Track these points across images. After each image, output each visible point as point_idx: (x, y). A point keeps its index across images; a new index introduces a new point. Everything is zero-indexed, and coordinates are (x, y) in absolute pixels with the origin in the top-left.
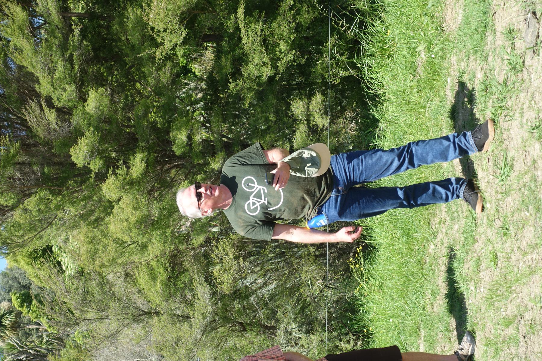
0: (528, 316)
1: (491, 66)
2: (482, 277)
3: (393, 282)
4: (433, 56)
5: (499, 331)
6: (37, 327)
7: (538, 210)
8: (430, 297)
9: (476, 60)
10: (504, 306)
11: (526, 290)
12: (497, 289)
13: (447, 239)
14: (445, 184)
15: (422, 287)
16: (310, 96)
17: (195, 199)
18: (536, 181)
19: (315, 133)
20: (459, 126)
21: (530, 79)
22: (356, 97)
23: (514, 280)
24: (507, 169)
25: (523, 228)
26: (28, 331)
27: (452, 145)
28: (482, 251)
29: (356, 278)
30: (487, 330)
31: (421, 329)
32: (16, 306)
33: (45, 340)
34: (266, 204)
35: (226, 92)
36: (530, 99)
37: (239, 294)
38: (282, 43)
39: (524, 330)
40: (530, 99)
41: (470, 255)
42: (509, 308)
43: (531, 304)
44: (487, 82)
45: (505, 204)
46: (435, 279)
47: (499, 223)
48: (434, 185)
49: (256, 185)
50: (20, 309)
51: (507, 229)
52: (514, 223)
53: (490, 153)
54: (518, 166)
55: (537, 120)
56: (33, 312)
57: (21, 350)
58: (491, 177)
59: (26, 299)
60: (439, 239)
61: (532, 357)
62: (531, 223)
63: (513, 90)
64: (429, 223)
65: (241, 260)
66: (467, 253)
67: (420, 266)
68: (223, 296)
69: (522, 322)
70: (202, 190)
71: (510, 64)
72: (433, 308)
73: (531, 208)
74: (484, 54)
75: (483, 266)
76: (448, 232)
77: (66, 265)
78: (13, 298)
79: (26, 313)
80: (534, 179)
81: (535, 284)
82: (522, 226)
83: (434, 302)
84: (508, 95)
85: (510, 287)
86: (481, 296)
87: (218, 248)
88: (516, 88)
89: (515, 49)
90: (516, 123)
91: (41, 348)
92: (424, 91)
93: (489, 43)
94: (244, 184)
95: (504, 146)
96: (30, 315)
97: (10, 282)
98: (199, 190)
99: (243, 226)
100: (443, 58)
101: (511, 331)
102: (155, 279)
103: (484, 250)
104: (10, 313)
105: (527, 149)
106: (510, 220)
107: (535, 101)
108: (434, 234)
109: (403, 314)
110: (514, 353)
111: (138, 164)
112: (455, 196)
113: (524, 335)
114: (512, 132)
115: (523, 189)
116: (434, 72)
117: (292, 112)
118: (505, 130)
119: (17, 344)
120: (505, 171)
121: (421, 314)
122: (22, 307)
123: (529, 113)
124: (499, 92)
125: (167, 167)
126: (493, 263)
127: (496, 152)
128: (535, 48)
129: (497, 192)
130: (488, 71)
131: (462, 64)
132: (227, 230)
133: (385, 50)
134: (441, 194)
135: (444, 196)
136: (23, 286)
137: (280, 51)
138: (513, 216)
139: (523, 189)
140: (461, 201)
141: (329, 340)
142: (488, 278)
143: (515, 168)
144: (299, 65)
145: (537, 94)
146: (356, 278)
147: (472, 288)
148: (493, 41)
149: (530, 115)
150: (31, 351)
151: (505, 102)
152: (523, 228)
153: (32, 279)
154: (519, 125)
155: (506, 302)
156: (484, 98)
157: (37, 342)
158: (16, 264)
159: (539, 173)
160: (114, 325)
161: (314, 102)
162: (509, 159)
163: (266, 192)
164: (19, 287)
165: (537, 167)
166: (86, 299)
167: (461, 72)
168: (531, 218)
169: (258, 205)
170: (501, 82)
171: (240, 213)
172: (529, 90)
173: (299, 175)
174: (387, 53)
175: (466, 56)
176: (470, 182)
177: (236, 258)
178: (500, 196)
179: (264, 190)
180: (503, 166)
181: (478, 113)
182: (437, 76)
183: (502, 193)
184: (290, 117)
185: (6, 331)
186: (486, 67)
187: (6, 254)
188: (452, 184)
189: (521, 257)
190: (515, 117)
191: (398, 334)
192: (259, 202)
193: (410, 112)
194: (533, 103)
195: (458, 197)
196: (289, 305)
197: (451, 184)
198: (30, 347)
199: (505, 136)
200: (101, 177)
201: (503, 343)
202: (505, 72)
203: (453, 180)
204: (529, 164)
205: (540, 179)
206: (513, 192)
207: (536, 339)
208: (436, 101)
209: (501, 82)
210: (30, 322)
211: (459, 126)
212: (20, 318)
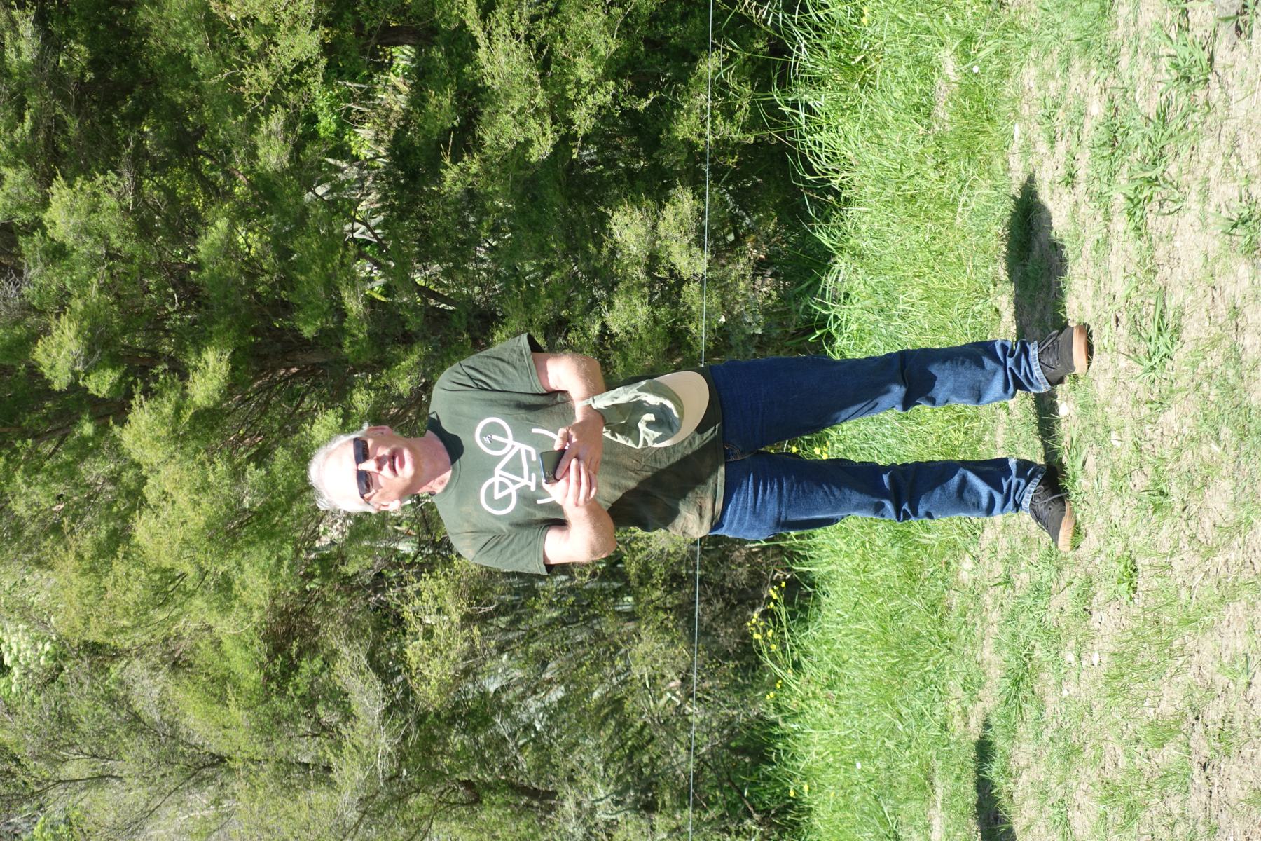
0: (1213, 713)
1: (1128, 81)
3: (865, 668)
4: (976, 69)
5: (1137, 761)
7: (1244, 434)
8: (960, 693)
9: (1087, 69)
10: (1151, 693)
11: (1208, 645)
12: (1136, 652)
13: (1005, 540)
14: (988, 472)
15: (940, 670)
16: (661, 197)
18: (1239, 360)
21: (1228, 100)
22: (778, 194)
24: (1167, 336)
28: (1098, 561)
31: (936, 779)
34: (533, 489)
36: (1228, 151)
39: (1203, 747)
40: (1228, 151)
41: (1066, 576)
43: (1222, 680)
44: (1117, 121)
46: (974, 645)
47: (1140, 481)
49: (510, 441)
51: (1162, 493)
54: (1194, 329)
55: (1244, 204)
60: (985, 543)
62: (1224, 472)
66: (1059, 569)
67: (935, 617)
69: (1199, 728)
70: (370, 466)
71: (1176, 66)
72: (966, 724)
73: (1226, 431)
74: (1107, 51)
75: (1101, 595)
77: (15, 651)
80: (1235, 356)
81: (1234, 627)
82: (1201, 480)
83: (971, 707)
85: (1168, 643)
88: (1191, 126)
89: (1188, 30)
90: (1191, 217)
92: (952, 164)
93: (1121, 23)
95: (1158, 280)
100: (1003, 74)
101: (1171, 753)
103: (1103, 556)
105: (1218, 281)
106: (1171, 470)
107: (1239, 156)
109: (890, 744)
111: (209, 376)
112: (1011, 504)
113: (1203, 760)
114: (1178, 244)
115: (1205, 385)
117: (611, 235)
118: (1161, 239)
123: (1223, 188)
124: (1146, 142)
125: (292, 361)
126: (1125, 586)
127: (1136, 300)
128: (1240, 18)
131: (1052, 84)
132: (437, 551)
133: (852, 69)
134: (977, 494)
135: (985, 502)
137: (579, 84)
138: (1178, 460)
139: (1205, 385)
143: (1184, 335)
144: (629, 114)
145: (1244, 137)
147: (1071, 657)
148: (1131, 16)
149: (1226, 193)
154: (1197, 223)
155: (1158, 682)
156: (1108, 163)
159: (1248, 340)
160: (137, 795)
162: (1170, 314)
165: (1241, 325)
167: (1049, 102)
169: (512, 490)
170: (1153, 116)
172: (1224, 129)
174: (855, 70)
179: (528, 453)
180: (1153, 332)
182: (986, 123)
183: (1152, 402)
189: (1197, 560)
190: (1187, 204)
191: (876, 799)
192: (515, 482)
193: (900, 280)
194: (1234, 160)
195: (1017, 507)
196: (592, 751)
197: (1007, 472)
199: (1160, 255)
200: (114, 410)
201: (1149, 788)
202: (1162, 87)
203: (1012, 463)
205: (1250, 356)
206: (1179, 396)
207: (1235, 768)
209: (1153, 116)
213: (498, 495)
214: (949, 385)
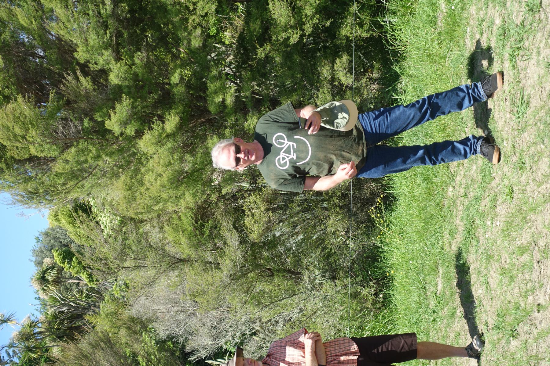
0: (542, 243)
1: (510, 11)
4: (453, 7)
5: (513, 260)
6: (78, 281)
9: (494, 7)
10: (519, 236)
11: (540, 218)
12: (513, 221)
17: (234, 163)
19: (339, 91)
20: (477, 72)
22: (380, 55)
23: (529, 210)
24: (524, 105)
25: (538, 160)
28: (499, 188)
29: (378, 225)
30: (503, 260)
32: (58, 263)
34: (295, 159)
35: (255, 59)
37: (271, 244)
38: (307, 7)
39: (537, 255)
41: (487, 193)
44: (506, 26)
45: (521, 140)
46: (453, 219)
49: (286, 142)
50: (62, 265)
51: (523, 163)
53: (507, 92)
54: (535, 103)
58: (508, 115)
59: (68, 255)
61: (545, 280)
62: (546, 155)
63: (530, 31)
64: (448, 168)
65: (270, 213)
66: (484, 191)
67: (439, 208)
68: (253, 244)
69: (536, 248)
70: (241, 156)
71: (528, 6)
75: (500, 200)
76: (466, 174)
77: (105, 224)
78: (55, 254)
79: (67, 269)
84: (525, 35)
85: (525, 218)
86: (497, 230)
88: (533, 28)
90: (533, 62)
94: (276, 140)
95: (521, 85)
96: (71, 270)
97: (52, 241)
98: (238, 155)
99: (274, 180)
100: (463, 9)
101: (526, 257)
103: (501, 186)
106: (526, 154)
108: (453, 178)
110: (528, 278)
113: (538, 260)
114: (528, 71)
115: (539, 123)
116: (454, 23)
120: (522, 108)
121: (440, 253)
122: (64, 263)
123: (545, 51)
124: (517, 34)
126: (509, 197)
129: (513, 130)
130: (506, 16)
131: (481, 13)
134: (459, 150)
137: (306, 15)
138: (529, 151)
139: (539, 123)
142: (504, 212)
143: (531, 105)
146: (378, 225)
147: (489, 223)
150: (72, 304)
151: (522, 43)
152: (538, 160)
154: (536, 64)
155: (521, 232)
160: (152, 273)
162: (525, 97)
163: (295, 147)
164: (61, 246)
166: (122, 255)
167: (480, 19)
168: (546, 150)
169: (287, 159)
171: (272, 167)
173: (328, 126)
175: (485, 4)
177: (267, 210)
178: (516, 133)
179: (293, 145)
180: (519, 104)
181: (496, 57)
186: (503, 12)
189: (536, 187)
190: (532, 57)
191: (417, 274)
192: (288, 157)
196: (315, 255)
198: (71, 300)
199: (522, 75)
201: (518, 270)
202: (523, 13)
204: (544, 100)
206: (529, 128)
208: (456, 51)
210: (71, 277)
211: (477, 72)
213: (282, 162)
214: (449, 106)
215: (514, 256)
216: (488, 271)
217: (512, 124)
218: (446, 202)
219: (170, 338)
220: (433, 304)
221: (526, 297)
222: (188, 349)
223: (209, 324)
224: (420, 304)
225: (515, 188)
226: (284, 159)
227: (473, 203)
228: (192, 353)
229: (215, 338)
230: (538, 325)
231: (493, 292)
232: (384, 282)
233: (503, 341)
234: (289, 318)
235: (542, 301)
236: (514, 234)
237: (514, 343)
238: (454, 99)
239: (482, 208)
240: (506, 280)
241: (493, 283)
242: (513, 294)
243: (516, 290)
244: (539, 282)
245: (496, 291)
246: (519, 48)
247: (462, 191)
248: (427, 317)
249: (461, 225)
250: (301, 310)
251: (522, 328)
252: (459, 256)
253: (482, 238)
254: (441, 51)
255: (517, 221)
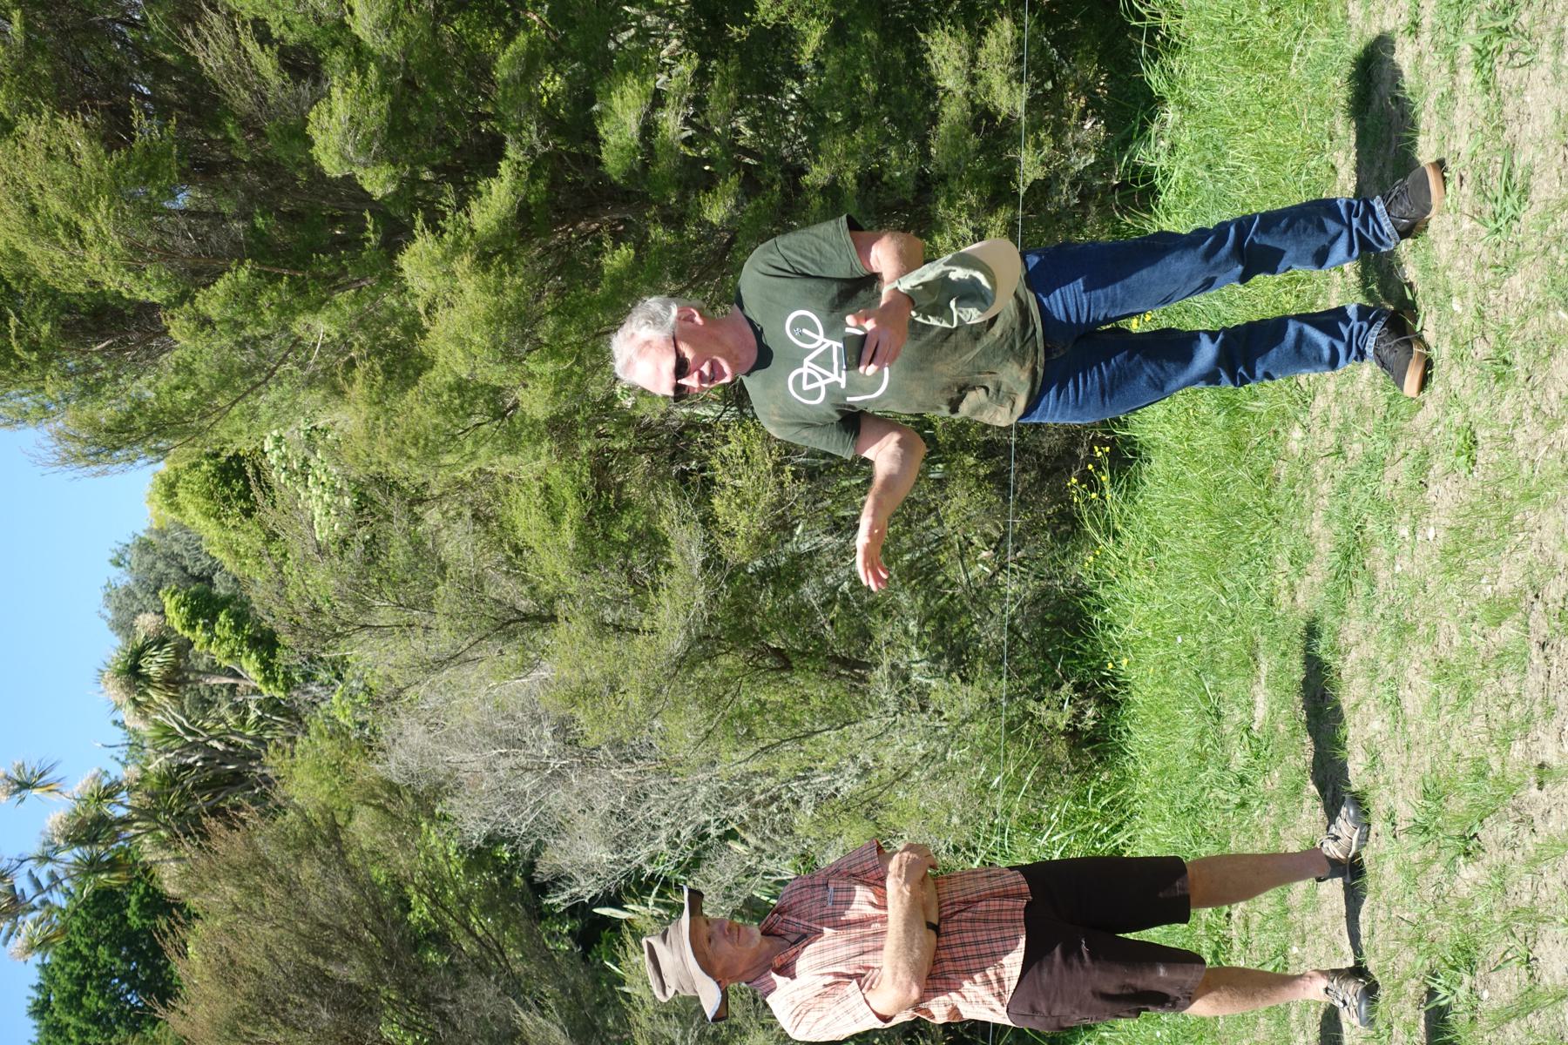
2: (1433, 499)
5: (1472, 639)
6: (232, 681)
10: (1489, 570)
15: (1266, 543)
24: (1514, 196)
26: (207, 695)
27: (1345, 235)
28: (1435, 431)
32: (177, 627)
33: (252, 717)
34: (843, 386)
39: (1542, 626)
41: (1402, 446)
42: (1504, 574)
45: (1502, 298)
47: (1482, 349)
48: (1299, 325)
49: (821, 337)
50: (187, 634)
51: (1505, 362)
52: (1524, 345)
56: (222, 642)
57: (189, 739)
58: (1467, 225)
59: (204, 606)
60: (1316, 412)
66: (1394, 440)
67: (1262, 488)
69: (1539, 606)
72: (1294, 599)
75: (1438, 467)
76: (1343, 390)
78: (169, 604)
86: (1428, 552)
87: (726, 441)
90: (1543, 70)
91: (241, 735)
95: (1506, 137)
96: (212, 650)
97: (160, 565)
98: (683, 381)
101: (1508, 632)
102: (555, 520)
103: (1440, 428)
104: (161, 642)
106: (1516, 338)
113: (1542, 640)
114: (1528, 99)
115: (1554, 248)
117: (928, 71)
118: (1510, 93)
119: (181, 725)
120: (1508, 204)
121: (1262, 616)
122: (192, 628)
126: (1464, 458)
129: (1481, 266)
134: (1318, 347)
135: (1326, 353)
136: (192, 576)
138: (1523, 327)
139: (1554, 248)
140: (1368, 370)
141: (1010, 698)
142: (1448, 500)
143: (1533, 196)
147: (1405, 531)
153: (217, 555)
157: (231, 721)
158: (174, 516)
161: (991, 42)
162: (1518, 173)
164: (185, 580)
169: (822, 383)
176: (1394, 318)
178: (1488, 275)
180: (1500, 193)
184: (921, 86)
185: (150, 691)
187: (158, 451)
188: (1347, 321)
189: (1541, 433)
190: (1540, 56)
191: (1197, 674)
192: (825, 377)
195: (1362, 355)
199: (1509, 110)
201: (1485, 667)
206: (1526, 261)
208: (1321, 37)
210: (214, 669)
212: (187, 660)
213: (806, 387)
215: (1475, 626)
216: (1400, 669)
217: (1477, 249)
218: (1283, 470)
219: (492, 840)
220: (1239, 758)
221: (1507, 743)
222: (544, 869)
223: (606, 807)
224: (1203, 757)
225: (1482, 434)
226: (812, 379)
227: (1361, 473)
228: (559, 880)
229: (621, 844)
230: (1538, 823)
231: (1412, 729)
232: (1108, 696)
233: (1438, 867)
234: (832, 789)
235: (1550, 756)
236: (1474, 565)
237: (1469, 873)
238: (1309, 226)
239: (1385, 489)
240: (1450, 696)
241: (1413, 702)
242: (1468, 736)
243: (1479, 723)
244: (1545, 700)
245: (1420, 726)
246: (1502, 32)
247: (1330, 439)
248: (1221, 794)
249: (1323, 535)
250: (866, 770)
251: (1493, 832)
252: (1312, 632)
253: (1383, 575)
254: (1278, 36)
255: (1486, 528)
